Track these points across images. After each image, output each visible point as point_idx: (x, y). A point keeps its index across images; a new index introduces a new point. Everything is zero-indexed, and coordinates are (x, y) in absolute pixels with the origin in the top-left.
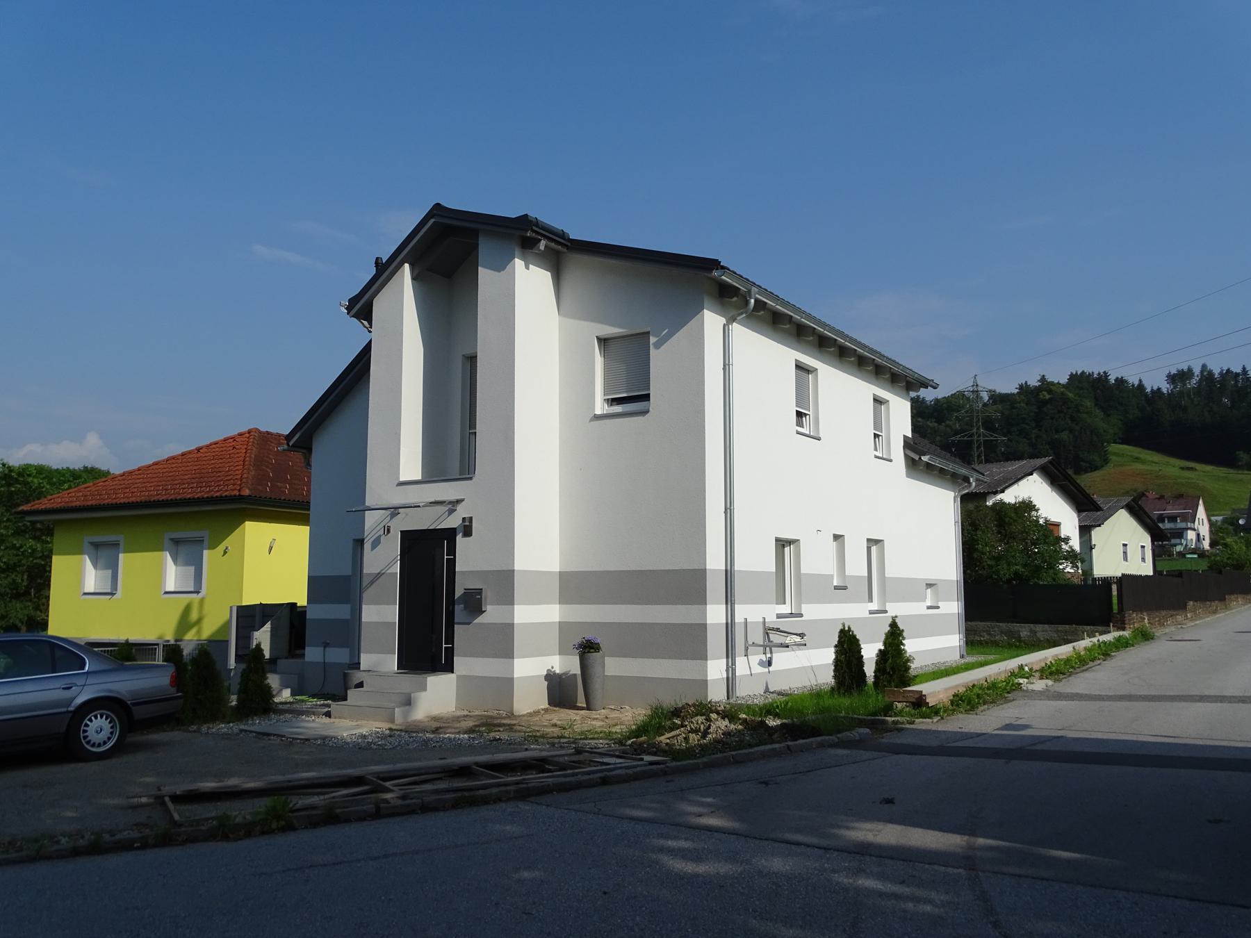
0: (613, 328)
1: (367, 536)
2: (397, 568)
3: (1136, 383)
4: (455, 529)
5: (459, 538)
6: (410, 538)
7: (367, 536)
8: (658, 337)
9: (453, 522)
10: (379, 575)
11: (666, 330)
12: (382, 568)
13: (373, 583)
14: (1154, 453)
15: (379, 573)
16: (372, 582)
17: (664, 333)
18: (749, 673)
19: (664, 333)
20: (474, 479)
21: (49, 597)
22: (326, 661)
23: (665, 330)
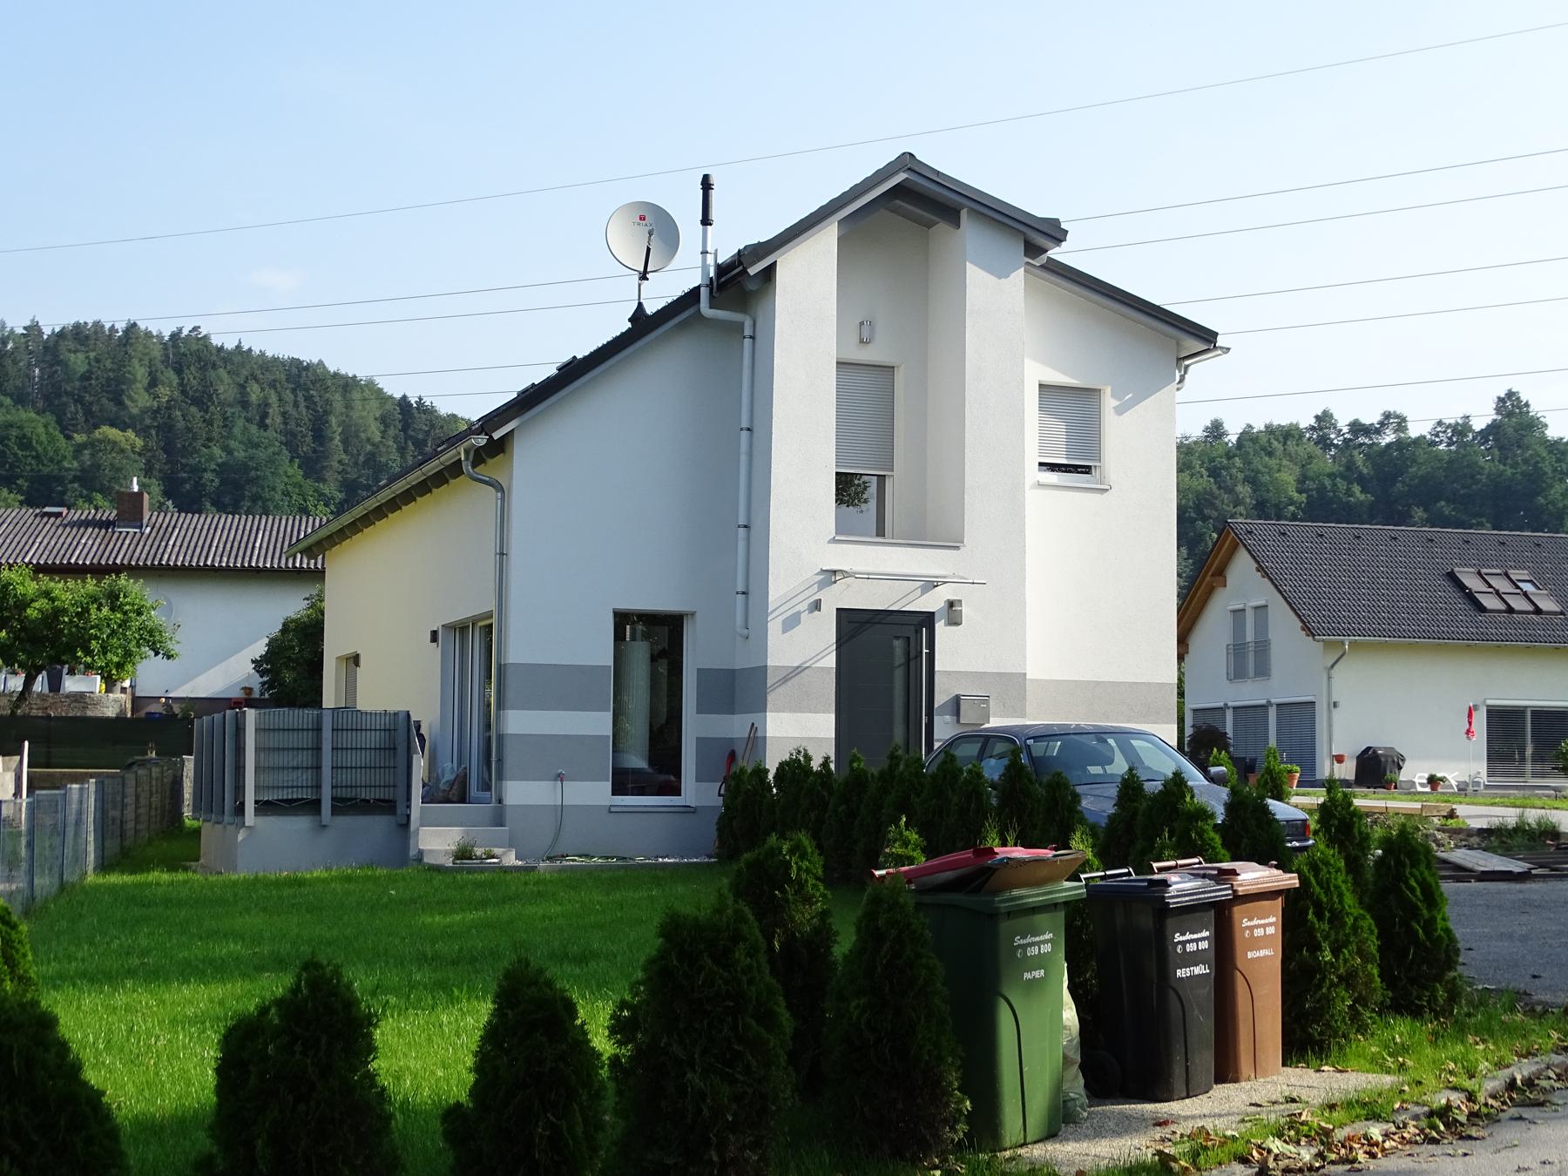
0: (1048, 370)
1: (772, 612)
2: (830, 661)
3: (242, 691)
4: (933, 614)
5: (940, 626)
6: (853, 624)
7: (772, 612)
8: (1121, 400)
9: (930, 602)
10: (798, 671)
11: (1130, 395)
12: (804, 660)
13: (787, 681)
14: (649, 684)
15: (798, 667)
16: (785, 680)
17: (1127, 397)
18: (564, 783)
19: (1127, 397)
20: (962, 549)
21: (1180, 471)
22: (559, 783)
23: (1128, 394)
